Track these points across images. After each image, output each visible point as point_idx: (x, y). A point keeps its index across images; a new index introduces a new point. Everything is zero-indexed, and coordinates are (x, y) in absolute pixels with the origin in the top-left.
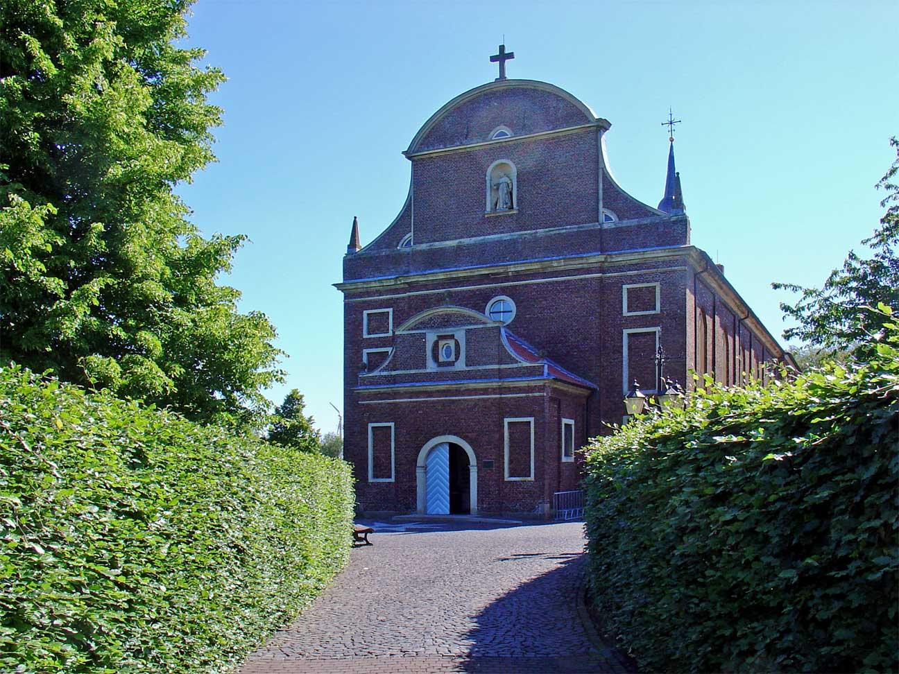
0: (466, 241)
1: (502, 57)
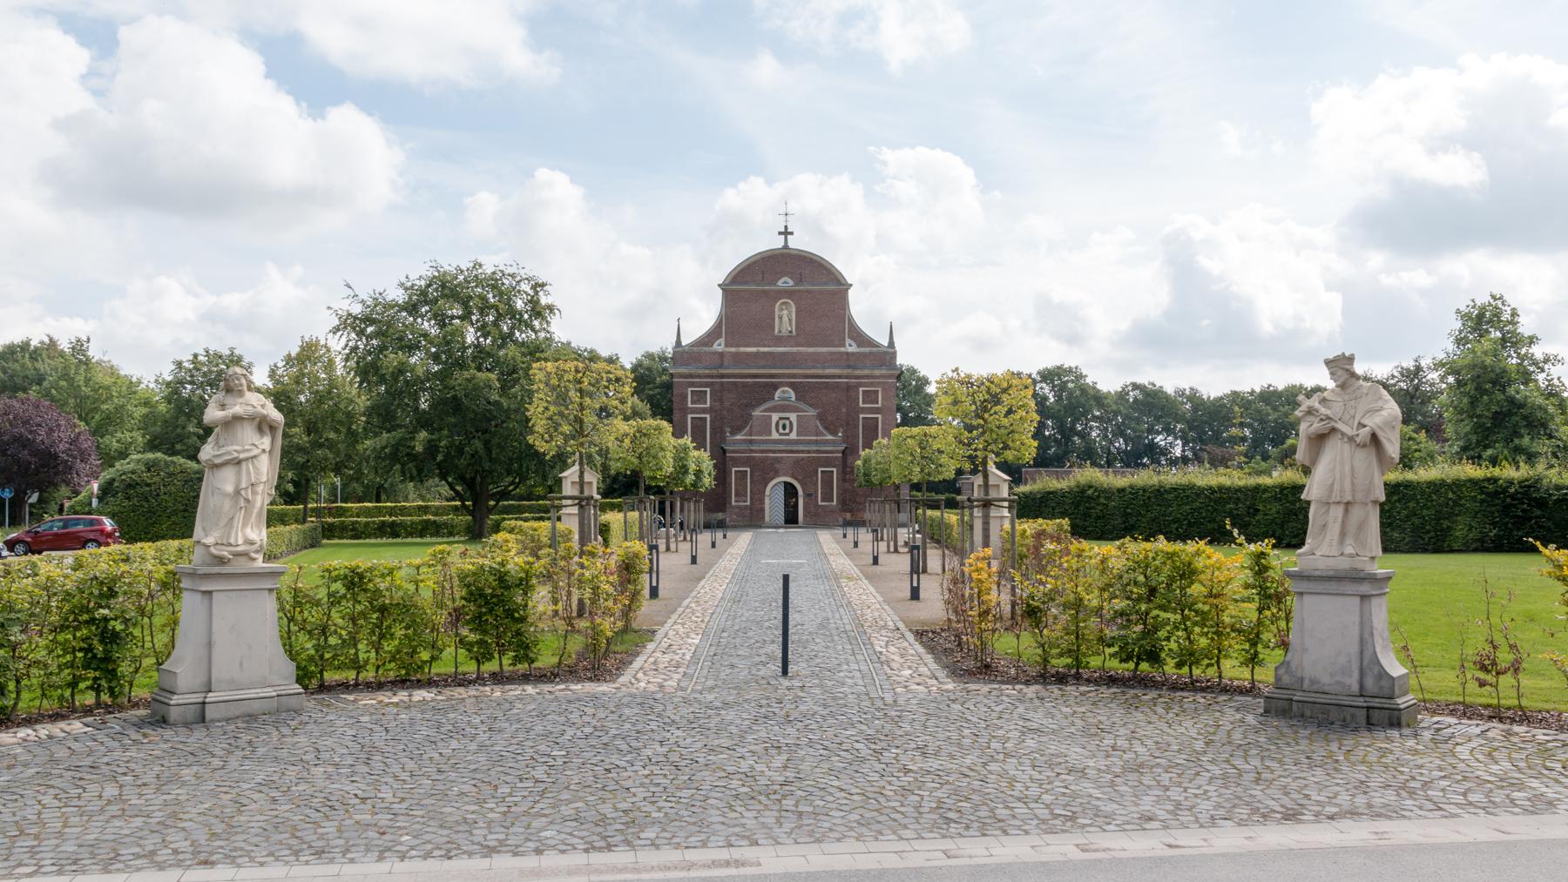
1: (786, 233)
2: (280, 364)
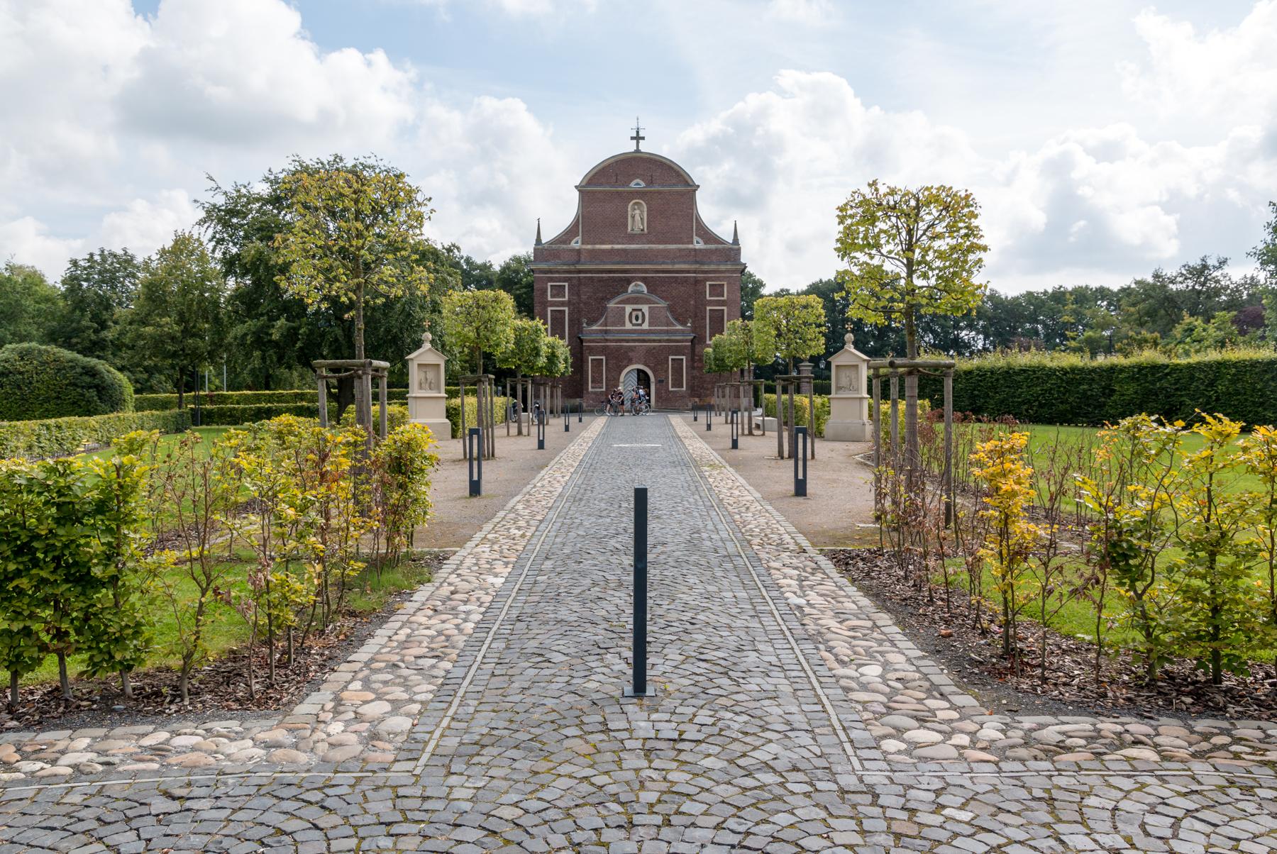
0: (617, 247)
1: (638, 138)
2: (155, 257)
